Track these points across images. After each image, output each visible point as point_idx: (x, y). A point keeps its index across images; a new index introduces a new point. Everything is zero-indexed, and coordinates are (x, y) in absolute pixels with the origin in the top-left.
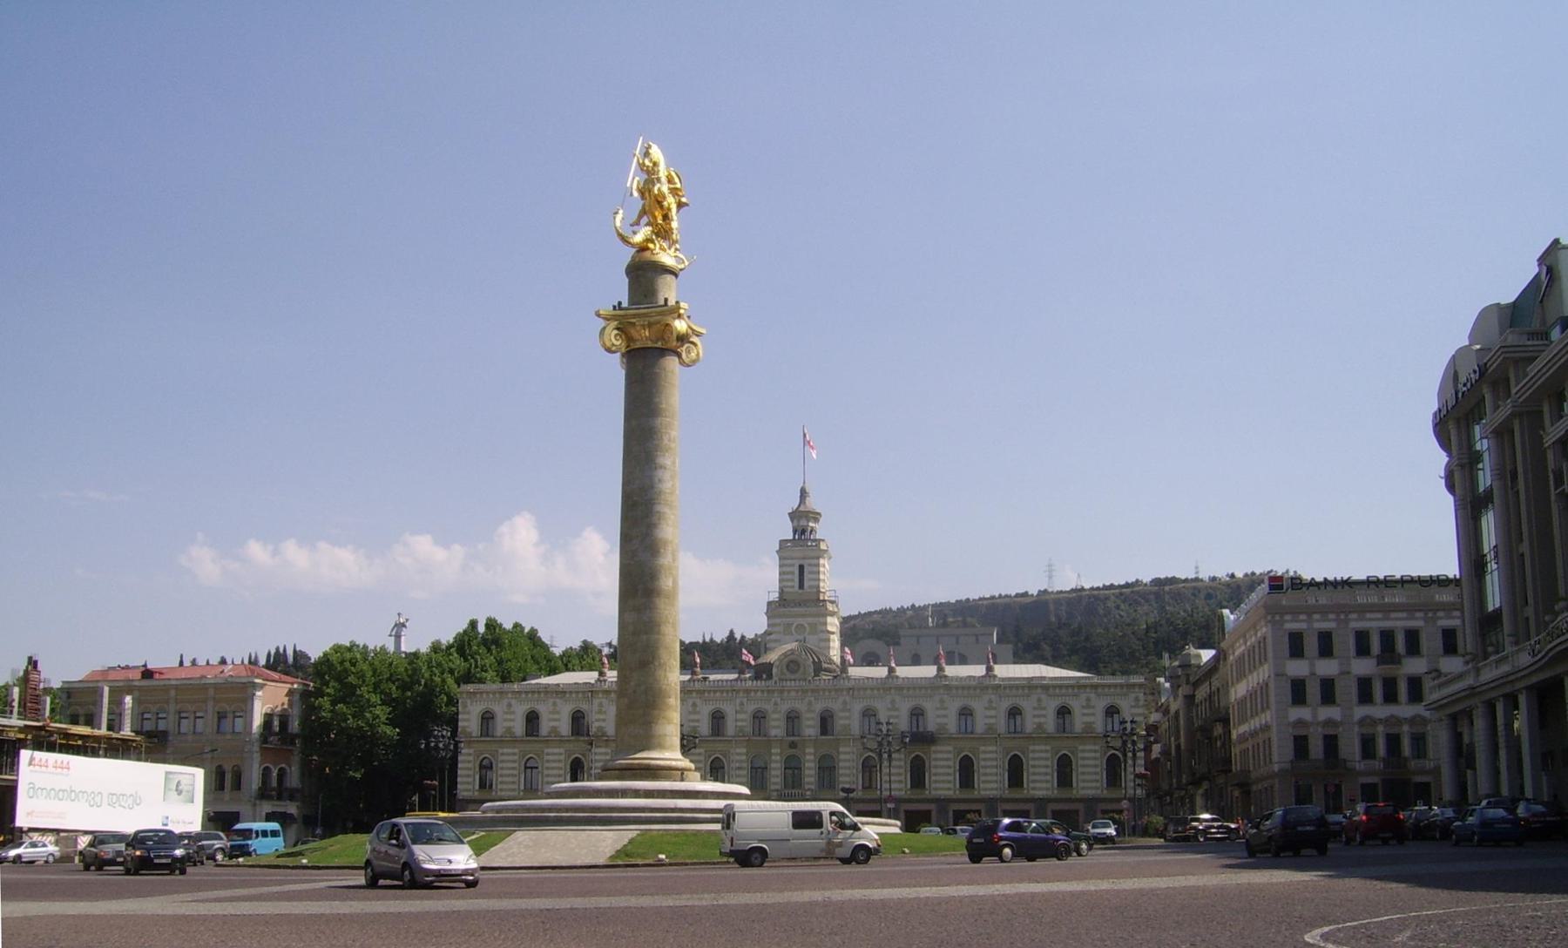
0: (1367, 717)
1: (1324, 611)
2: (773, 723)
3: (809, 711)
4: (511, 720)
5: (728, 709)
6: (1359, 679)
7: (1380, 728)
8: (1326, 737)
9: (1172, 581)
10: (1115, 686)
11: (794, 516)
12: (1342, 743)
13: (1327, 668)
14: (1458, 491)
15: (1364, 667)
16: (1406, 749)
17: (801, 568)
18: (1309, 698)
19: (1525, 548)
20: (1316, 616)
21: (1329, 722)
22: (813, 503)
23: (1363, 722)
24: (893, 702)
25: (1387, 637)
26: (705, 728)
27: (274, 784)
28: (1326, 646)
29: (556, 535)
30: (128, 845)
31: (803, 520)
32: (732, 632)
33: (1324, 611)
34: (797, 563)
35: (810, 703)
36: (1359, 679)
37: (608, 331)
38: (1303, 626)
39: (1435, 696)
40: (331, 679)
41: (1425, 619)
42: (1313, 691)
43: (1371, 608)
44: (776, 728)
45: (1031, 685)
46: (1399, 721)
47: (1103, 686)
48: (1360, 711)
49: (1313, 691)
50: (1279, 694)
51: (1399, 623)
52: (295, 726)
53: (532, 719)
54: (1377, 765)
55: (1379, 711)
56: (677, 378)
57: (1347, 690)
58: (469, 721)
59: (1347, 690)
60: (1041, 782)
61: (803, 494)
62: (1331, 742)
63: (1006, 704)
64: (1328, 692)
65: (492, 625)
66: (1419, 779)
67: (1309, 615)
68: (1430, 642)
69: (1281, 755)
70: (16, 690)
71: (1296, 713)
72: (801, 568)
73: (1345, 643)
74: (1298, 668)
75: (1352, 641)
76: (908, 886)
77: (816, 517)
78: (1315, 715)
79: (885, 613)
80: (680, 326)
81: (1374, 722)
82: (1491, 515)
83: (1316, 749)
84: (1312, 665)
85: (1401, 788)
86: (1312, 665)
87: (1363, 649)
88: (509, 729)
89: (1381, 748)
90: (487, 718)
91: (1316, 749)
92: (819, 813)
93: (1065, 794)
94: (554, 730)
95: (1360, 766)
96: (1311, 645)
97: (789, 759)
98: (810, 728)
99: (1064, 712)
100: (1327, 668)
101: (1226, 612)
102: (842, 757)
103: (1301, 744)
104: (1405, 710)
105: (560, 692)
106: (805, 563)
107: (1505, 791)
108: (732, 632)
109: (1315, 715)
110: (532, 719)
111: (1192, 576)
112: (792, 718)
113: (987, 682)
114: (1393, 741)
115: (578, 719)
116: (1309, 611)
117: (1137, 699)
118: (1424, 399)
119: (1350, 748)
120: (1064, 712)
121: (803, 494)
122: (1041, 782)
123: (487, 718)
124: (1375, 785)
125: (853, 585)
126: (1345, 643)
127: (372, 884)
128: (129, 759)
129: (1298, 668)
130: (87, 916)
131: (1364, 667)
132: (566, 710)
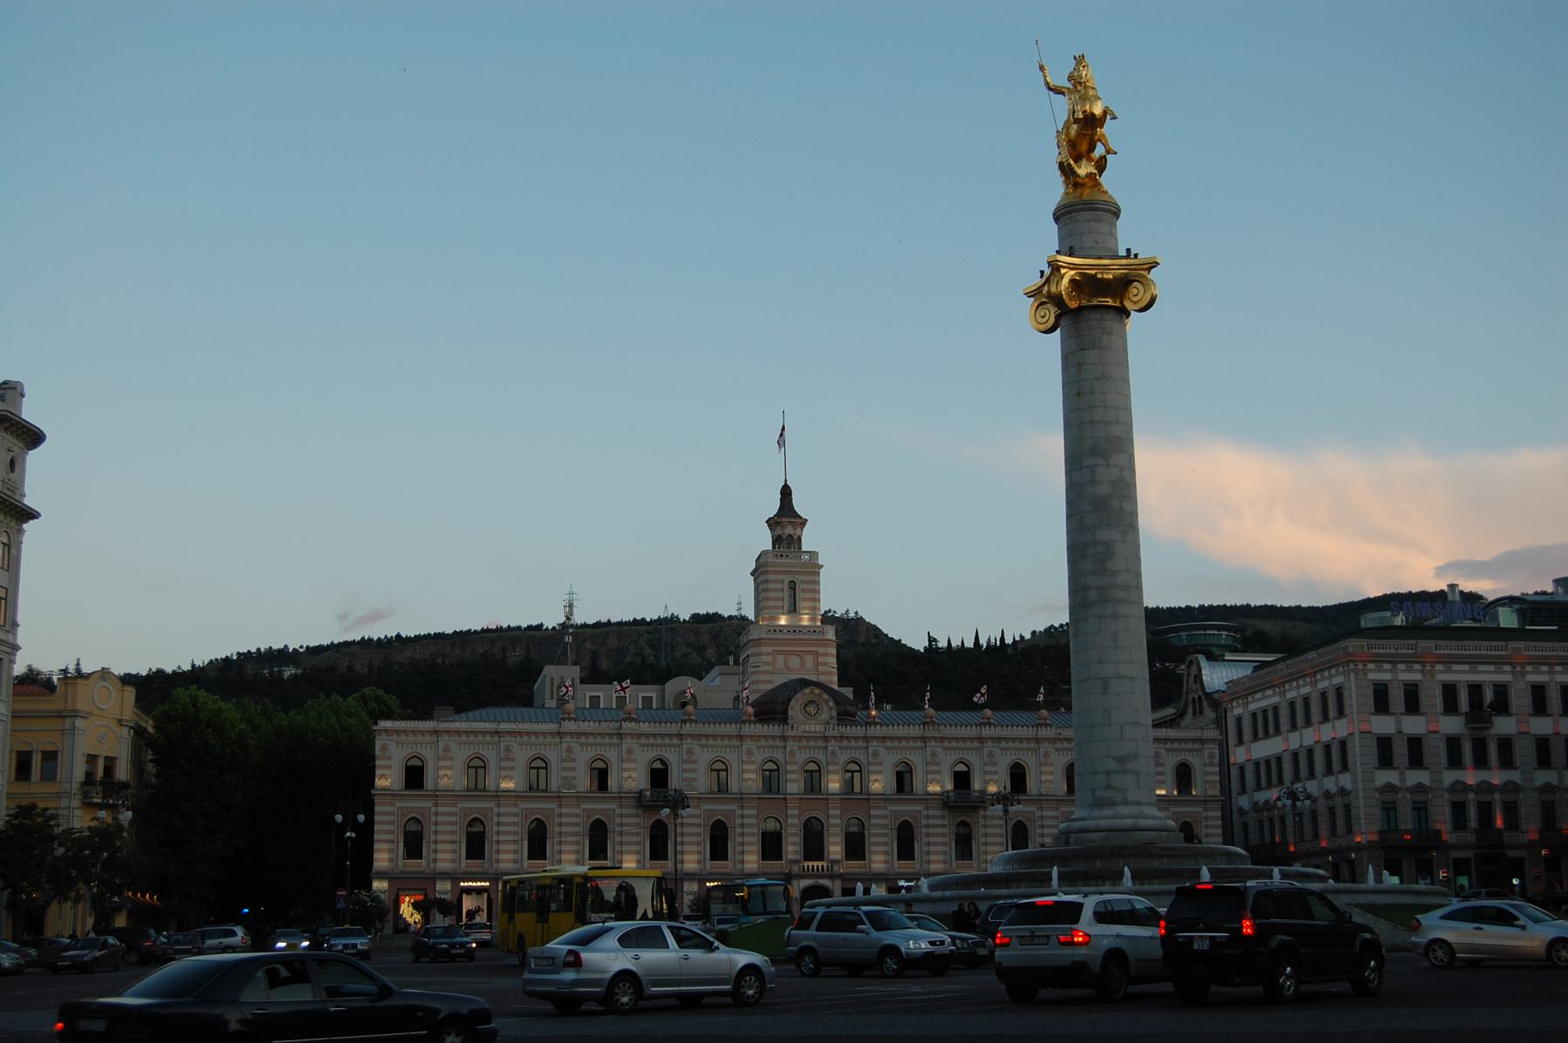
0: (1484, 782)
6: (764, 859)
7: (1497, 796)
10: (483, 733)
11: (772, 523)
13: (1414, 725)
14: (211, 701)
15: (1452, 725)
17: (793, 586)
18: (1518, 760)
20: (1401, 666)
21: (1420, 788)
24: (569, 750)
25: (1476, 690)
27: (100, 773)
28: (1413, 703)
29: (796, 853)
30: (1522, 614)
31: (786, 521)
36: (764, 859)
38: (1386, 676)
40: (428, 836)
41: (1513, 673)
42: (1401, 752)
44: (794, 785)
48: (1450, 777)
49: (1401, 752)
50: (1363, 753)
51: (1487, 676)
52: (123, 773)
54: (1471, 838)
55: (1471, 777)
57: (1436, 751)
59: (1436, 751)
61: (786, 492)
62: (1421, 809)
65: (398, 636)
66: (1513, 854)
67: (1551, 665)
68: (1520, 700)
71: (1384, 777)
73: (1432, 698)
78: (1403, 780)
82: (309, 998)
83: (1406, 820)
84: (1398, 721)
85: (543, 914)
86: (1398, 721)
87: (1450, 706)
90: (414, 776)
91: (1406, 820)
95: (1449, 837)
96: (1397, 699)
97: (808, 825)
98: (794, 785)
100: (1414, 725)
101: (151, 730)
102: (873, 831)
103: (1389, 809)
104: (1496, 777)
106: (797, 578)
108: (1153, 265)
109: (1403, 780)
114: (1485, 810)
117: (1211, 756)
121: (786, 492)
122: (508, 855)
123: (414, 776)
124: (1468, 860)
126: (1432, 698)
128: (1128, 411)
129: (1383, 725)
131: (1452, 725)
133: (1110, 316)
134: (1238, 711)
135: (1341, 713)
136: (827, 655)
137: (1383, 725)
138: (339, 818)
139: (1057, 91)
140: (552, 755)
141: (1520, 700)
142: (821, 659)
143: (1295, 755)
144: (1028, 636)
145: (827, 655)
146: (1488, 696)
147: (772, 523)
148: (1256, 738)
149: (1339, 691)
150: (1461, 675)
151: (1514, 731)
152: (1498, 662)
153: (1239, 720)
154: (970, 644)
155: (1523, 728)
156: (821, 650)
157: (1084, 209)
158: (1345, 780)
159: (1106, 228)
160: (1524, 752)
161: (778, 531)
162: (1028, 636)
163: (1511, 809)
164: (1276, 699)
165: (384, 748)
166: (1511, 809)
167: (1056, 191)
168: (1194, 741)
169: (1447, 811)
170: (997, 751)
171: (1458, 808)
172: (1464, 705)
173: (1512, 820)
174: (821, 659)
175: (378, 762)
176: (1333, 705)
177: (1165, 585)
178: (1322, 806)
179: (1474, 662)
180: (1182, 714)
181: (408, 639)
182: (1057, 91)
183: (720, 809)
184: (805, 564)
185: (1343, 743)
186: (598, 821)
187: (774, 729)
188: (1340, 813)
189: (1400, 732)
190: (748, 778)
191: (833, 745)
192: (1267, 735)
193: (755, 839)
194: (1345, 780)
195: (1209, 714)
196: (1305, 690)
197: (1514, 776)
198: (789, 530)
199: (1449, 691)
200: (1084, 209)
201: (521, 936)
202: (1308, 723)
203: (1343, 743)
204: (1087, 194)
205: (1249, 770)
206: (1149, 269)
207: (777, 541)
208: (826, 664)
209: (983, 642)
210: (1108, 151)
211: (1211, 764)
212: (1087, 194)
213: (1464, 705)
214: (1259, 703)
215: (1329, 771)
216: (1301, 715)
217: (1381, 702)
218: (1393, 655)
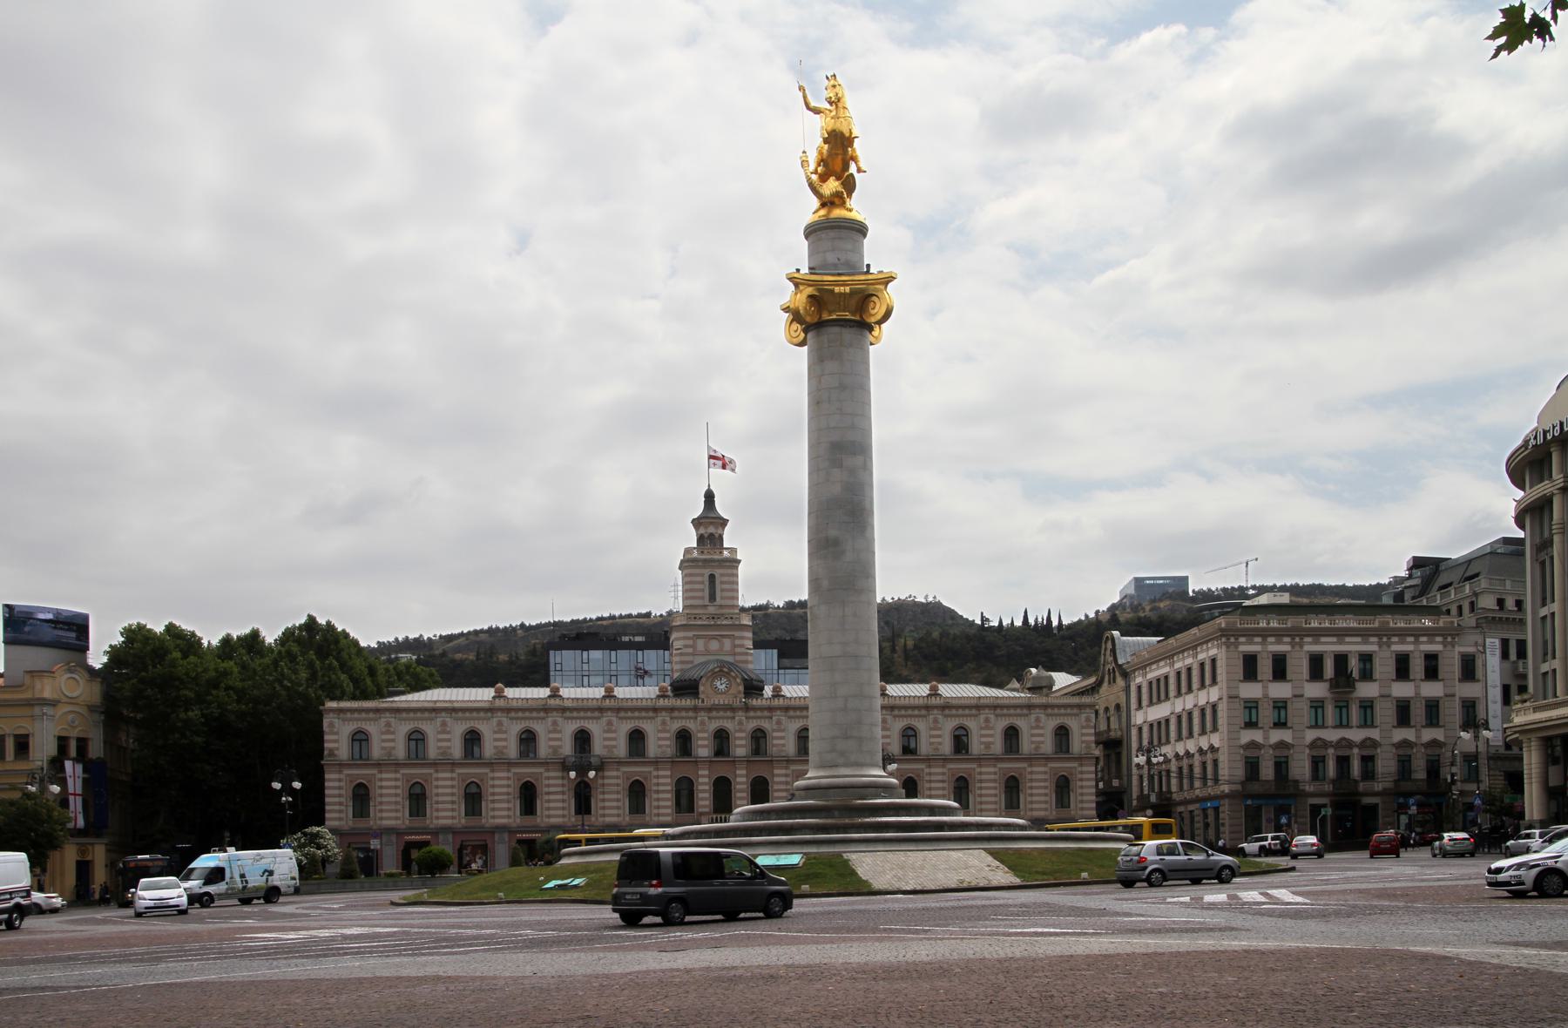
0: (1344, 739)
1: (1430, 633)
2: (669, 796)
3: (740, 731)
4: (388, 739)
5: (648, 727)
7: (1331, 751)
8: (588, 811)
9: (952, 614)
11: (697, 523)
12: (1292, 764)
15: (1317, 690)
16: (1356, 768)
17: (712, 577)
19: (99, 916)
21: (1282, 745)
22: (721, 509)
23: (1314, 744)
25: (1341, 660)
26: (895, 749)
28: (1280, 672)
31: (710, 524)
32: (1552, 39)
33: (1278, 634)
34: (707, 572)
35: (703, 723)
37: (879, 317)
38: (1410, 648)
39: (335, 824)
42: (1418, 713)
43: (1417, 634)
44: (740, 748)
45: (978, 706)
46: (1349, 744)
47: (680, 709)
51: (1353, 647)
53: (417, 739)
54: (1328, 788)
56: (887, 351)
57: (1300, 713)
58: (337, 738)
59: (1300, 713)
60: (501, 810)
61: (709, 497)
62: (1281, 766)
63: (1002, 724)
64: (1433, 710)
69: (1230, 770)
70: (1249, 802)
71: (1247, 736)
72: (712, 577)
73: (1299, 666)
74: (1251, 691)
75: (1305, 664)
76: (375, 982)
77: (723, 523)
78: (1418, 737)
79: (491, 631)
80: (936, 634)
81: (1325, 744)
83: (1267, 772)
84: (1265, 688)
86: (1265, 688)
87: (1316, 672)
88: (555, 750)
89: (1331, 769)
90: (360, 738)
91: (1267, 772)
92: (676, 696)
93: (418, 823)
94: (500, 751)
95: (1309, 788)
98: (740, 748)
99: (1012, 734)
103: (1252, 767)
105: (453, 710)
106: (717, 572)
107: (1145, 743)
109: (1418, 737)
110: (417, 739)
111: (664, 597)
112: (722, 737)
113: (934, 701)
114: (1343, 762)
115: (472, 739)
116: (1264, 634)
117: (1088, 720)
118: (1158, 570)
119: (1300, 768)
120: (1012, 734)
121: (709, 497)
123: (360, 738)
125: (1065, 622)
126: (1299, 666)
127: (631, 919)
129: (1251, 691)
130: (1256, 951)
131: (1366, 690)
132: (459, 729)
133: (848, 334)
134: (1139, 680)
135: (1214, 682)
136: (743, 638)
137: (1402, 690)
138: (297, 785)
139: (817, 111)
140: (1021, 724)
141: (1384, 666)
142: (737, 642)
143: (1179, 717)
144: (1092, 615)
145: (743, 638)
146: (1354, 665)
147: (697, 523)
148: (1151, 703)
149: (1214, 661)
150: (1329, 647)
151: (1441, 694)
152: (1364, 634)
153: (1139, 688)
154: (1018, 623)
155: (1385, 692)
156: (737, 634)
157: (835, 232)
158: (1215, 740)
159: (849, 246)
160: (1385, 713)
161: (702, 531)
162: (1092, 615)
163: (1367, 760)
164: (1166, 670)
165: (331, 725)
166: (1367, 760)
167: (808, 209)
168: (687, 709)
169: (1307, 765)
170: (560, 720)
171: (1317, 763)
172: (1329, 669)
173: (1369, 774)
174: (737, 642)
175: (326, 737)
176: (1208, 675)
177: (898, 576)
178: (1197, 760)
179: (1341, 634)
180: (1099, 684)
181: (531, 627)
182: (817, 111)
183: (637, 771)
184: (727, 560)
185: (1214, 706)
186: (361, 785)
187: (687, 702)
188: (1185, 771)
189: (1266, 696)
190: (659, 742)
191: (740, 715)
192: (1159, 701)
193: (669, 796)
194: (1215, 740)
195: (1120, 682)
196: (1189, 661)
197: (1374, 734)
198: (711, 530)
199: (1316, 662)
200: (835, 232)
201: (1490, 884)
202: (1190, 690)
203: (1214, 706)
204: (838, 213)
205: (1145, 730)
206: (886, 284)
207: (701, 539)
208: (742, 646)
209: (1032, 621)
210: (859, 170)
211: (1088, 727)
212: (838, 213)
213: (1329, 669)
214: (1155, 673)
215: (1203, 732)
216: (1185, 682)
217: (1402, 668)
218: (1263, 629)
